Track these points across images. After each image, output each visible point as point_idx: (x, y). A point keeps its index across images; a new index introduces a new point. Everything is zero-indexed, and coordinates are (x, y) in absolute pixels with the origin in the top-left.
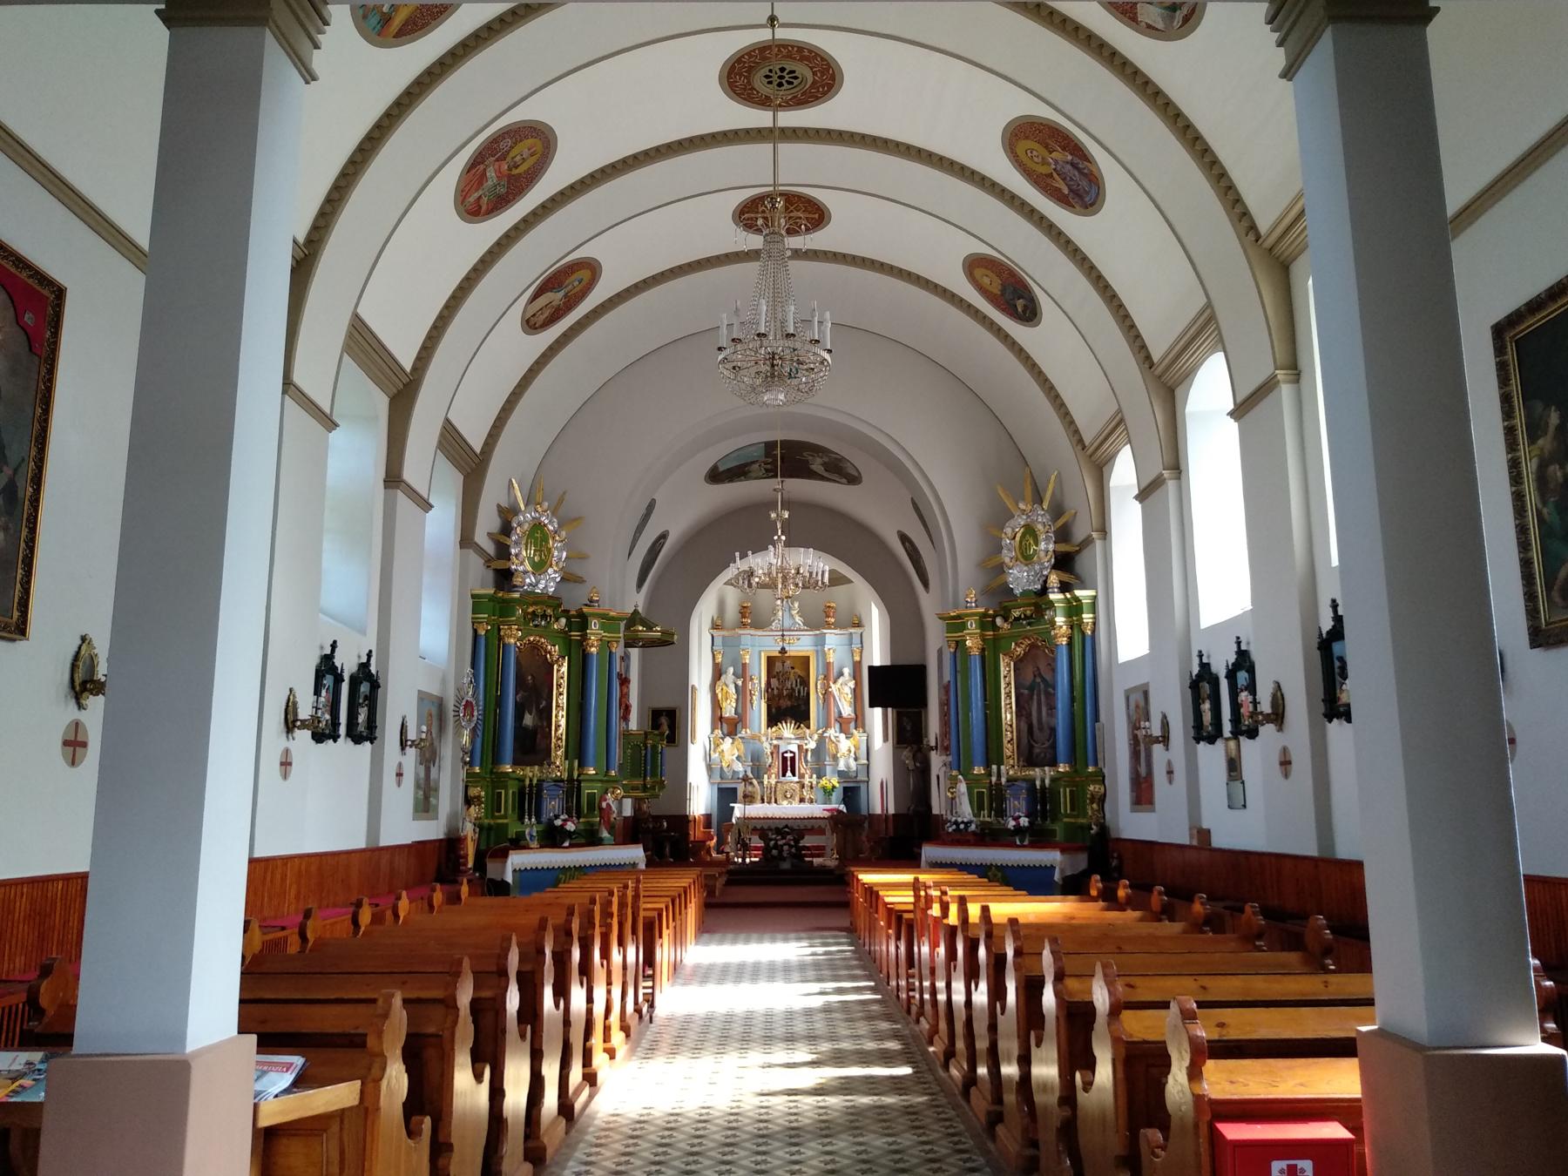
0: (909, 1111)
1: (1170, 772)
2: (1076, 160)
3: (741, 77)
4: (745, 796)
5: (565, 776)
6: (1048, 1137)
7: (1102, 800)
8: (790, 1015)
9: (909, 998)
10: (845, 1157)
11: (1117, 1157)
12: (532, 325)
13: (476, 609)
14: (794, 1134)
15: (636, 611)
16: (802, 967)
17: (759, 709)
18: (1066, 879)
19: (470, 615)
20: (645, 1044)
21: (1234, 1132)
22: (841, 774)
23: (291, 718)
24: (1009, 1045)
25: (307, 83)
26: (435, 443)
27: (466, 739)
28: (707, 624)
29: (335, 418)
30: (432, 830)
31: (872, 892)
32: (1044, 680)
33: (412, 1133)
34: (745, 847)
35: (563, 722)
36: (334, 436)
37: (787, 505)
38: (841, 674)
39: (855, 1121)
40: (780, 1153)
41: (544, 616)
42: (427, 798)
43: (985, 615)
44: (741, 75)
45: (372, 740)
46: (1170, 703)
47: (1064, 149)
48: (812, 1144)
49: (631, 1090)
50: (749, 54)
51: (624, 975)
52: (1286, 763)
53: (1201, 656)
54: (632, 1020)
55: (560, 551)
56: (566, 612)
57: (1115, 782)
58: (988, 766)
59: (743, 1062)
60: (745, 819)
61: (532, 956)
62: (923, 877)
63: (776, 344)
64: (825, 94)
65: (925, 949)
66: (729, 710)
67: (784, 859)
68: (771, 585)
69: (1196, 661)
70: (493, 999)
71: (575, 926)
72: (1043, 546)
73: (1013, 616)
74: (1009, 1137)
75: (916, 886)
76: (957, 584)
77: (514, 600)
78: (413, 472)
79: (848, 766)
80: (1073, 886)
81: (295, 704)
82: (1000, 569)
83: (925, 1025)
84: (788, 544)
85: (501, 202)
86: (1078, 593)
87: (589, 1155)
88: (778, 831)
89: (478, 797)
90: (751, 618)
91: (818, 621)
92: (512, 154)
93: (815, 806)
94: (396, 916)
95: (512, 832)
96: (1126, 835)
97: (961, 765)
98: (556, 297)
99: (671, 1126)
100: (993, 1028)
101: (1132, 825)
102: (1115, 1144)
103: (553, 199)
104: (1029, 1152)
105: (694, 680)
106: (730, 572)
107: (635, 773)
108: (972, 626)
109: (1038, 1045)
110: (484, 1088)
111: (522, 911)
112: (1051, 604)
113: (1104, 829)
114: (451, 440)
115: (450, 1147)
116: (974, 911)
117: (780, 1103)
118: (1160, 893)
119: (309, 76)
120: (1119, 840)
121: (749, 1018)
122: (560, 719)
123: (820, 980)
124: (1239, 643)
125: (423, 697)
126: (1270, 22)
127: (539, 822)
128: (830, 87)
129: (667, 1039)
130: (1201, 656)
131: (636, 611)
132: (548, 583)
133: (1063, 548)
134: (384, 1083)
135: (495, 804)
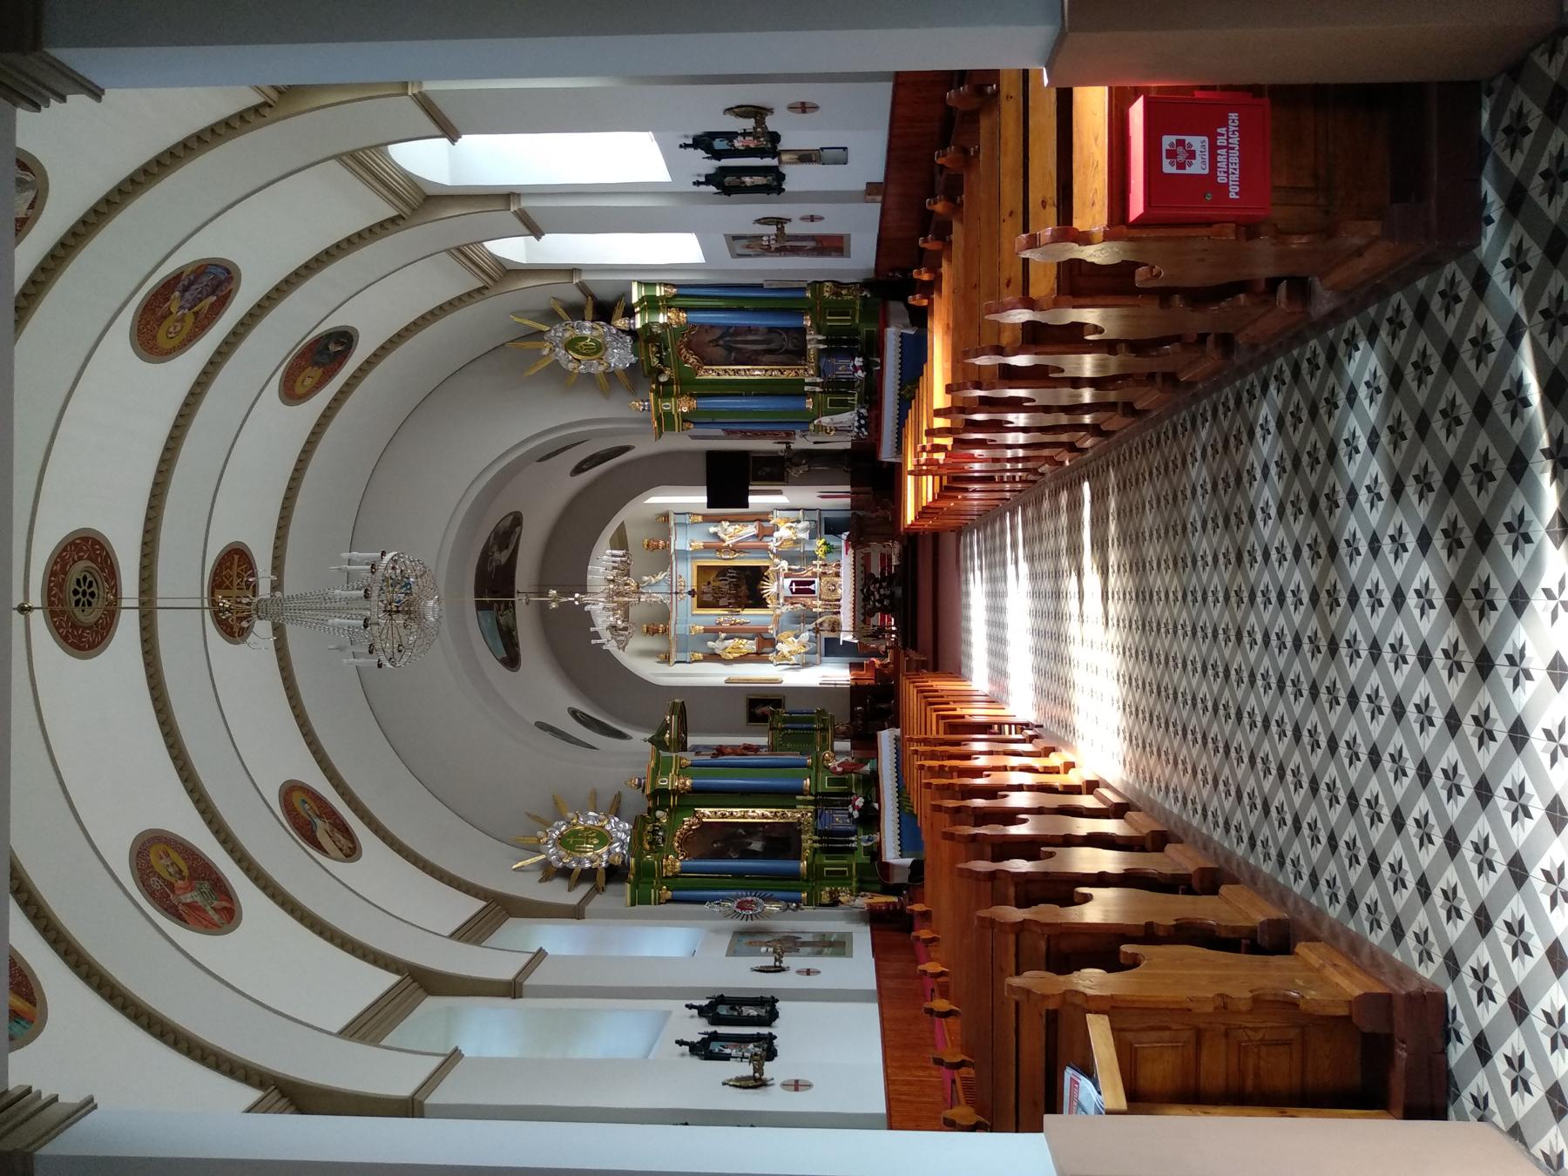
0: (1123, 487)
1: (812, 219)
2: (180, 286)
3: (83, 633)
4: (833, 630)
5: (811, 808)
6: (1145, 364)
7: (837, 284)
8: (1036, 594)
9: (1021, 481)
10: (1162, 549)
11: (1161, 306)
12: (351, 851)
13: (645, 901)
14: (1142, 596)
15: (651, 741)
16: (992, 580)
17: (750, 616)
18: (913, 324)
19: (652, 907)
20: (1061, 733)
21: (1137, 207)
22: (812, 537)
23: (752, 1083)
24: (1064, 396)
25: (95, 1107)
26: (476, 948)
27: (774, 908)
28: (664, 668)
29: (449, 1052)
30: (862, 938)
31: (922, 513)
32: (721, 337)
33: (1134, 963)
34: (879, 633)
35: (759, 811)
36: (468, 1051)
37: (542, 592)
38: (715, 535)
39: (1131, 539)
40: (1159, 610)
41: (654, 832)
42: (831, 944)
43: (657, 393)
44: (81, 636)
45: (774, 1001)
46: (745, 215)
47: (168, 299)
48: (1151, 579)
49: (1101, 750)
50: (57, 628)
51: (998, 753)
52: (804, 108)
53: (697, 183)
54: (1040, 745)
55: (588, 818)
56: (651, 811)
57: (821, 271)
58: (806, 395)
59: (1078, 640)
60: (856, 630)
61: (977, 846)
62: (910, 467)
63: (375, 610)
64: (103, 548)
65: (977, 466)
66: (750, 646)
67: (893, 593)
68: (626, 607)
69: (703, 188)
70: (1016, 885)
71: (951, 803)
72: (587, 333)
73: (658, 364)
74: (1146, 398)
75: (918, 474)
76: (625, 419)
77: (637, 864)
78: (503, 968)
79: (805, 529)
80: (920, 318)
81: (738, 1079)
82: (611, 375)
83: (1045, 468)
84: (584, 592)
85: (220, 887)
86: (635, 299)
87: (1159, 789)
88: (866, 599)
89: (831, 893)
90: (658, 625)
91: (662, 557)
92: (165, 875)
93: (843, 562)
94: (942, 974)
95: (865, 859)
96: (872, 264)
97: (804, 421)
98: (321, 828)
99: (1133, 711)
100: (1047, 409)
101: (862, 257)
102: (1151, 308)
103: (216, 833)
104: (1159, 379)
105: (720, 681)
106: (611, 646)
107: (811, 741)
108: (668, 405)
109: (1062, 371)
110: (1097, 892)
111: (938, 855)
112: (646, 327)
113: (866, 284)
114: (472, 932)
115: (1149, 925)
116: (939, 423)
117: (1114, 608)
118: (926, 241)
119: (89, 1105)
120: (877, 270)
121: (1038, 633)
122: (756, 814)
123: (1004, 564)
124: (686, 146)
125: (732, 952)
126: (39, 109)
127: (854, 833)
128: (96, 542)
129: (1057, 711)
130: (697, 183)
131: (651, 741)
132: (620, 830)
133: (589, 312)
134: (1089, 992)
135: (838, 877)
